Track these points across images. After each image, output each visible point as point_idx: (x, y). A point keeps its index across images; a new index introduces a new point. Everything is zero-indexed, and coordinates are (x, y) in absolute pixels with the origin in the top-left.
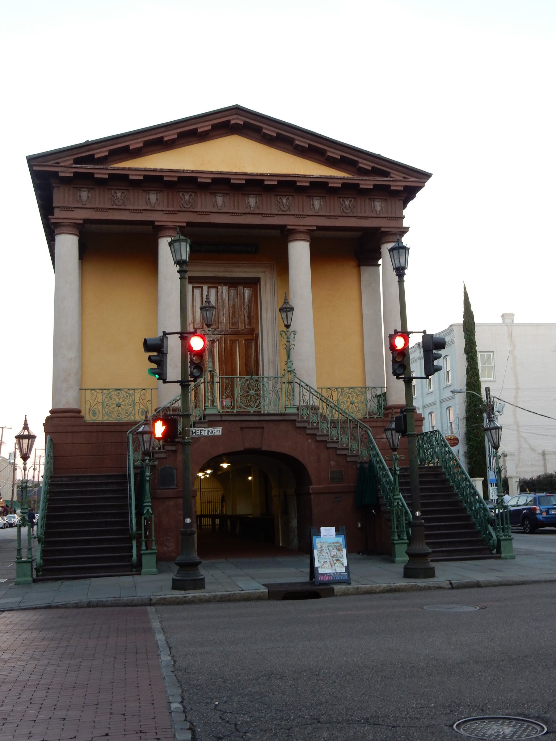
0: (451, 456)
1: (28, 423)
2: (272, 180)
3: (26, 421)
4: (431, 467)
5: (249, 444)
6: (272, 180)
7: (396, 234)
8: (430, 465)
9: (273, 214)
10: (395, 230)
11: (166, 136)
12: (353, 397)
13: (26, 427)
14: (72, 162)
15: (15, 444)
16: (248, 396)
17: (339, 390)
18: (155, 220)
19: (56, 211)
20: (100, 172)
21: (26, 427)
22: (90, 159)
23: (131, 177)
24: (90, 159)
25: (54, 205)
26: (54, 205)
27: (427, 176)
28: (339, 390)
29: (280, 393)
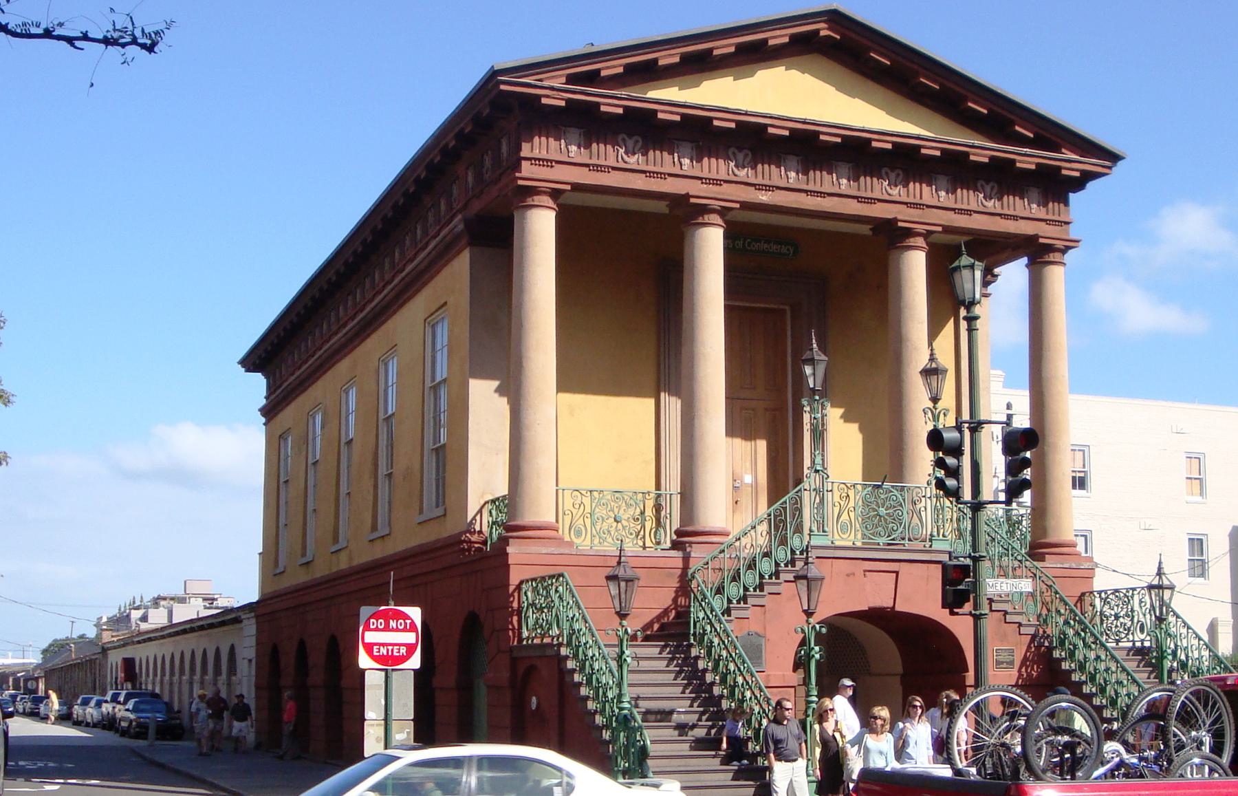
0: (408, 622)
1: (1163, 565)
2: (672, 113)
3: (1160, 563)
4: (548, 644)
5: (883, 600)
6: (672, 113)
7: (1059, 250)
8: (545, 641)
9: (551, 161)
10: (1059, 244)
11: (717, 48)
12: (619, 507)
13: (1160, 573)
14: (563, 80)
15: (210, 600)
16: (874, 510)
17: (595, 494)
18: (900, 217)
19: (525, 164)
20: (612, 103)
21: (1160, 573)
22: (592, 78)
23: (603, 108)
24: (592, 78)
25: (523, 154)
26: (523, 154)
27: (1114, 158)
28: (595, 494)
29: (923, 514)
